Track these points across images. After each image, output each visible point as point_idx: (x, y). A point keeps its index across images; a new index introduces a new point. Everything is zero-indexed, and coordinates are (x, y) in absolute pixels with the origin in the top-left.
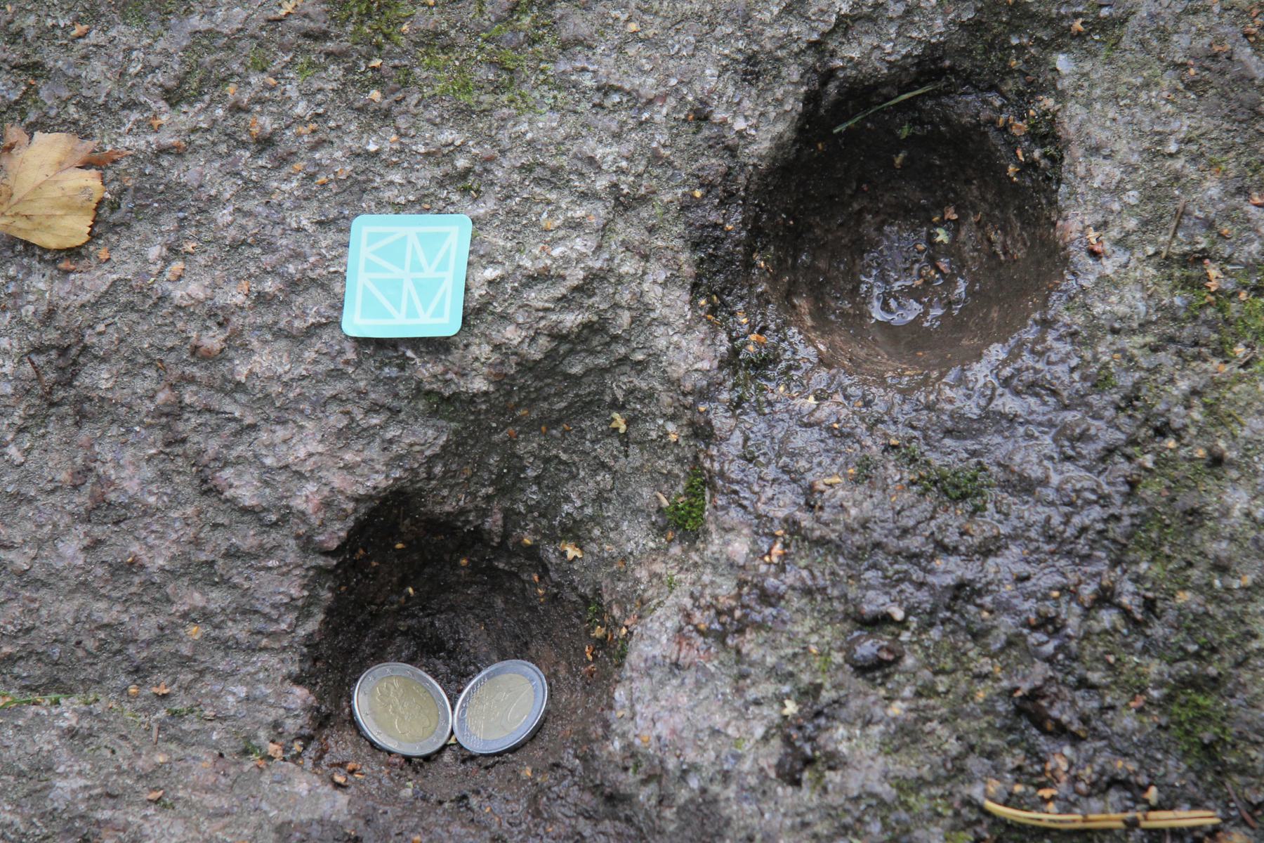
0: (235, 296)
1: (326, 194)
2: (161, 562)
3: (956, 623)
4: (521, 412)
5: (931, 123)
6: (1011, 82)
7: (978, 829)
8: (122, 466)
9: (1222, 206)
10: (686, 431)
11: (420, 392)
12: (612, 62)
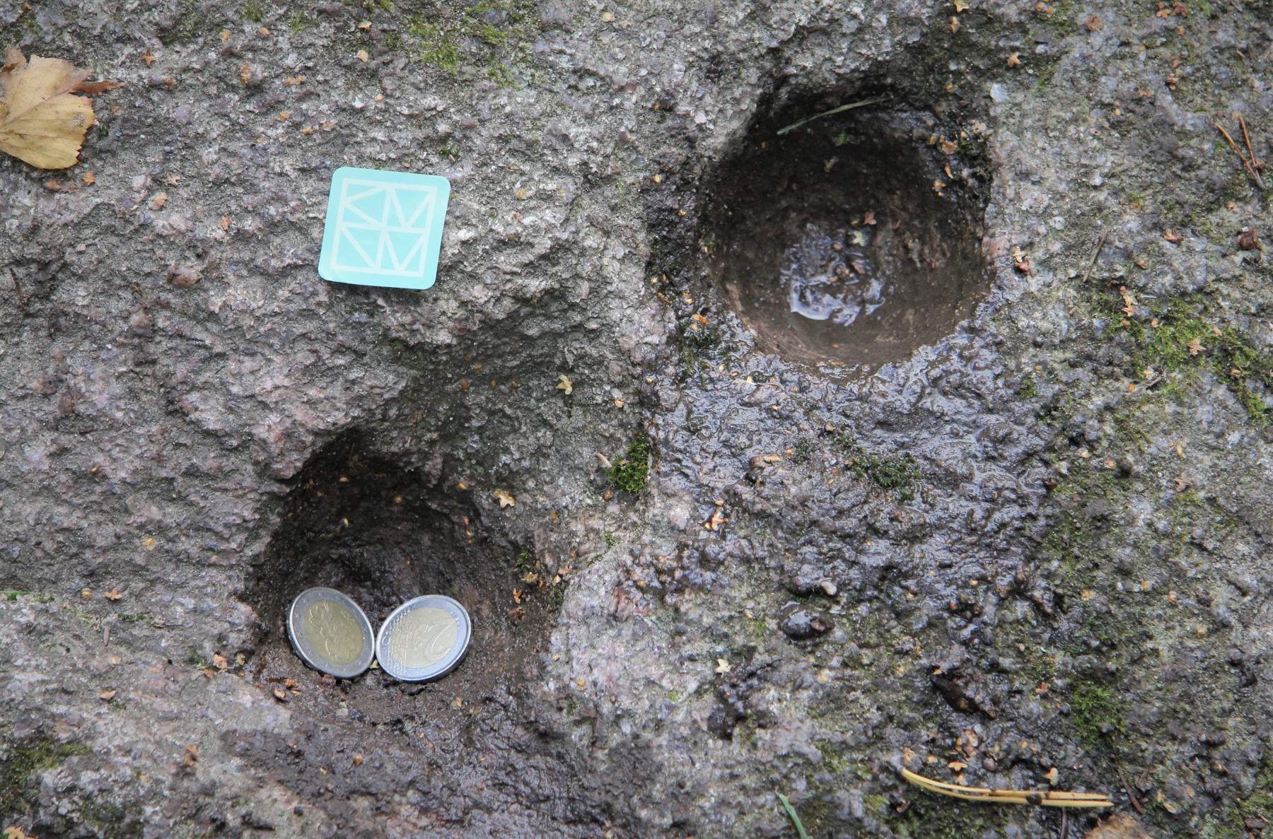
0: (215, 230)
1: (310, 144)
2: (123, 474)
3: (883, 602)
4: (475, 366)
5: (866, 134)
6: (944, 104)
7: (896, 795)
8: (92, 381)
9: (1139, 239)
10: (631, 399)
11: (386, 338)
12: (588, 48)
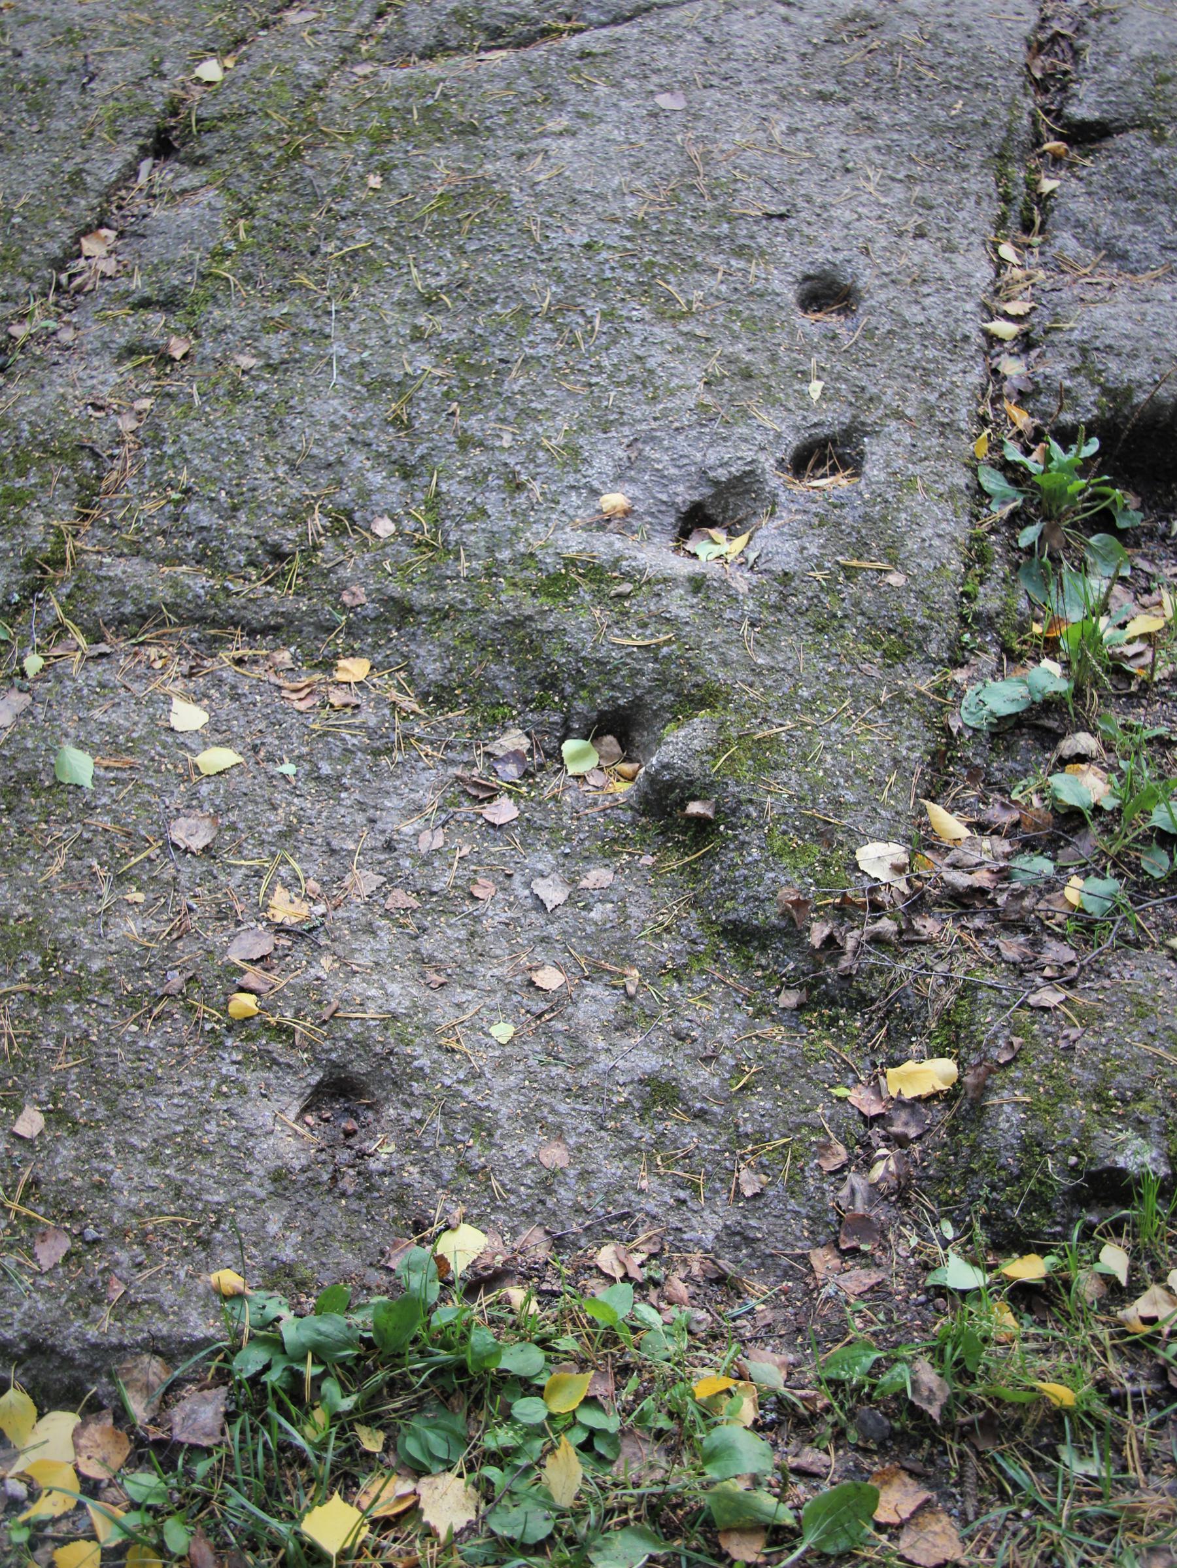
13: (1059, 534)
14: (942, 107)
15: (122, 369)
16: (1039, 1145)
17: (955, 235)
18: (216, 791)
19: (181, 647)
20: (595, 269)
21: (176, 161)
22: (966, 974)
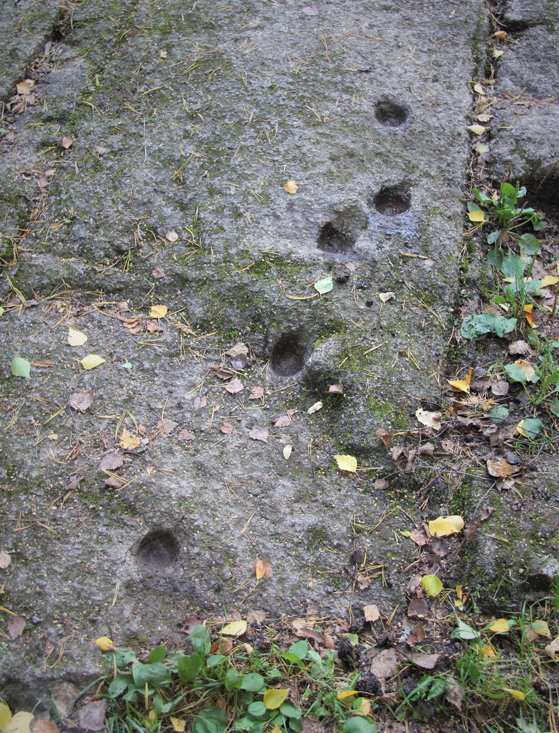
0: (313, 199)
13: (506, 234)
14: (445, 13)
15: (39, 154)
16: (505, 562)
17: (453, 80)
18: (92, 378)
19: (73, 301)
20: (275, 100)
21: (64, 43)
22: (467, 470)
